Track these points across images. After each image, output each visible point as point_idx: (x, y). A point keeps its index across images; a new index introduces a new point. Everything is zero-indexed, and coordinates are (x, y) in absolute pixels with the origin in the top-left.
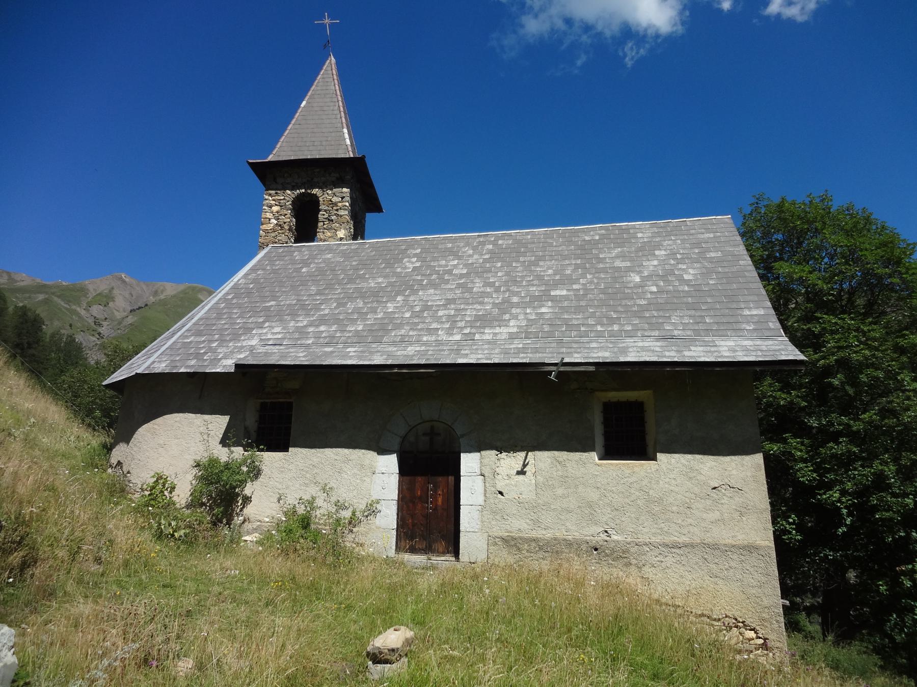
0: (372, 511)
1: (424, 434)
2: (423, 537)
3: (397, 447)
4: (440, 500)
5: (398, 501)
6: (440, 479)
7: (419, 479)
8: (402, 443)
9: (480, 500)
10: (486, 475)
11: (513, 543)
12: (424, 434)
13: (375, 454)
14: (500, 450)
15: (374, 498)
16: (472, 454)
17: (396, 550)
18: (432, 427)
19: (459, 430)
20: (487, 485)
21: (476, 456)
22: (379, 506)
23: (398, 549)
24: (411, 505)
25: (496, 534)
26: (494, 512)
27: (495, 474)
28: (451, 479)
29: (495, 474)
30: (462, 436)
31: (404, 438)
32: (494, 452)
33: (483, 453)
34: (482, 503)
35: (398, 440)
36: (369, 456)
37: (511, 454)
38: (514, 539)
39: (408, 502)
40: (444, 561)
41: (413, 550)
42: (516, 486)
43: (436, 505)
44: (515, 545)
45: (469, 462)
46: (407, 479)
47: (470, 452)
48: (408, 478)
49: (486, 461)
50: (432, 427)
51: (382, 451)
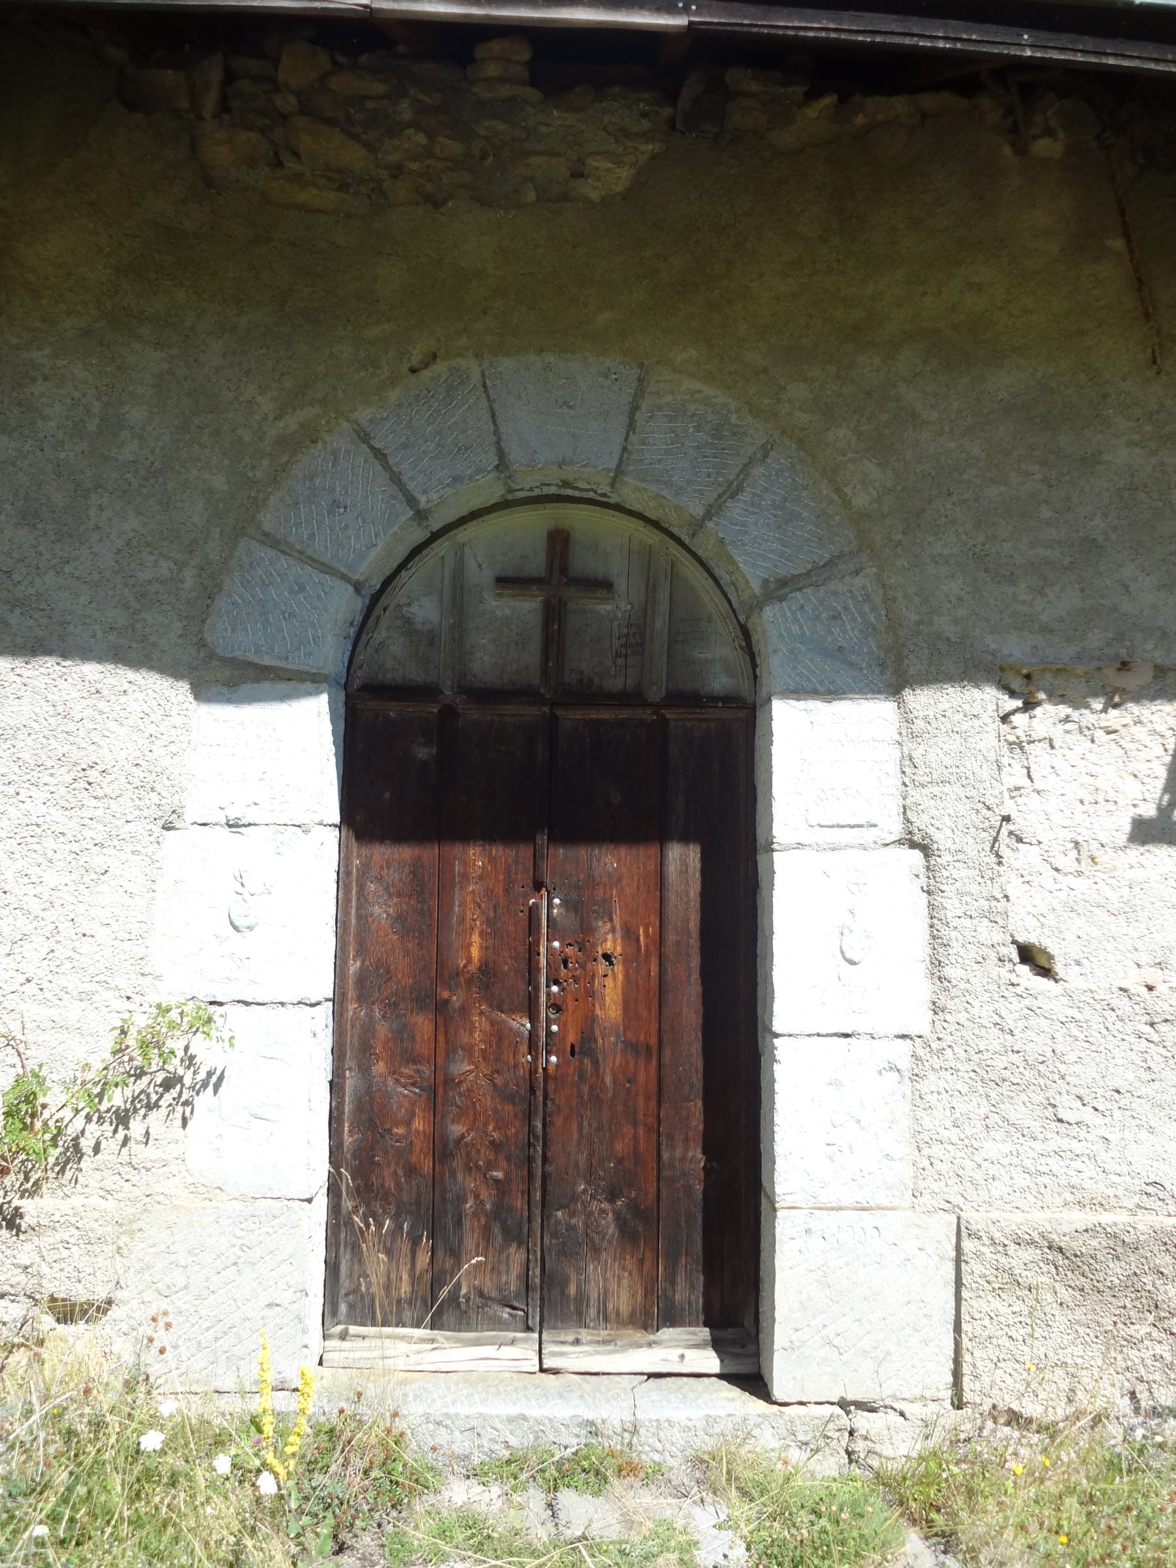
0: (155, 1078)
1: (506, 582)
2: (506, 1227)
3: (330, 653)
4: (611, 990)
5: (339, 1000)
6: (610, 861)
7: (475, 858)
8: (361, 631)
9: (907, 1001)
10: (942, 839)
11: (1116, 1272)
12: (506, 582)
13: (178, 692)
14: (1025, 685)
15: (178, 984)
16: (774, 713)
17: (330, 1311)
18: (559, 542)
19: (753, 545)
20: (952, 906)
21: (868, 719)
22: (208, 1054)
23: (348, 1301)
24: (423, 1024)
25: (1014, 1221)
26: (986, 1078)
27: (1003, 833)
28: (683, 861)
29: (1003, 833)
30: (779, 588)
31: (376, 600)
32: (987, 700)
33: (920, 699)
34: (920, 1023)
35: (340, 606)
36: (135, 703)
37: (1094, 714)
38: (1120, 1244)
39: (398, 1005)
40: (645, 1385)
41: (439, 1307)
42: (1128, 912)
43: (590, 1020)
44: (1132, 1284)
45: (825, 760)
46: (394, 858)
47: (831, 693)
48: (406, 853)
49: (935, 754)
50: (559, 542)
51: (227, 676)
